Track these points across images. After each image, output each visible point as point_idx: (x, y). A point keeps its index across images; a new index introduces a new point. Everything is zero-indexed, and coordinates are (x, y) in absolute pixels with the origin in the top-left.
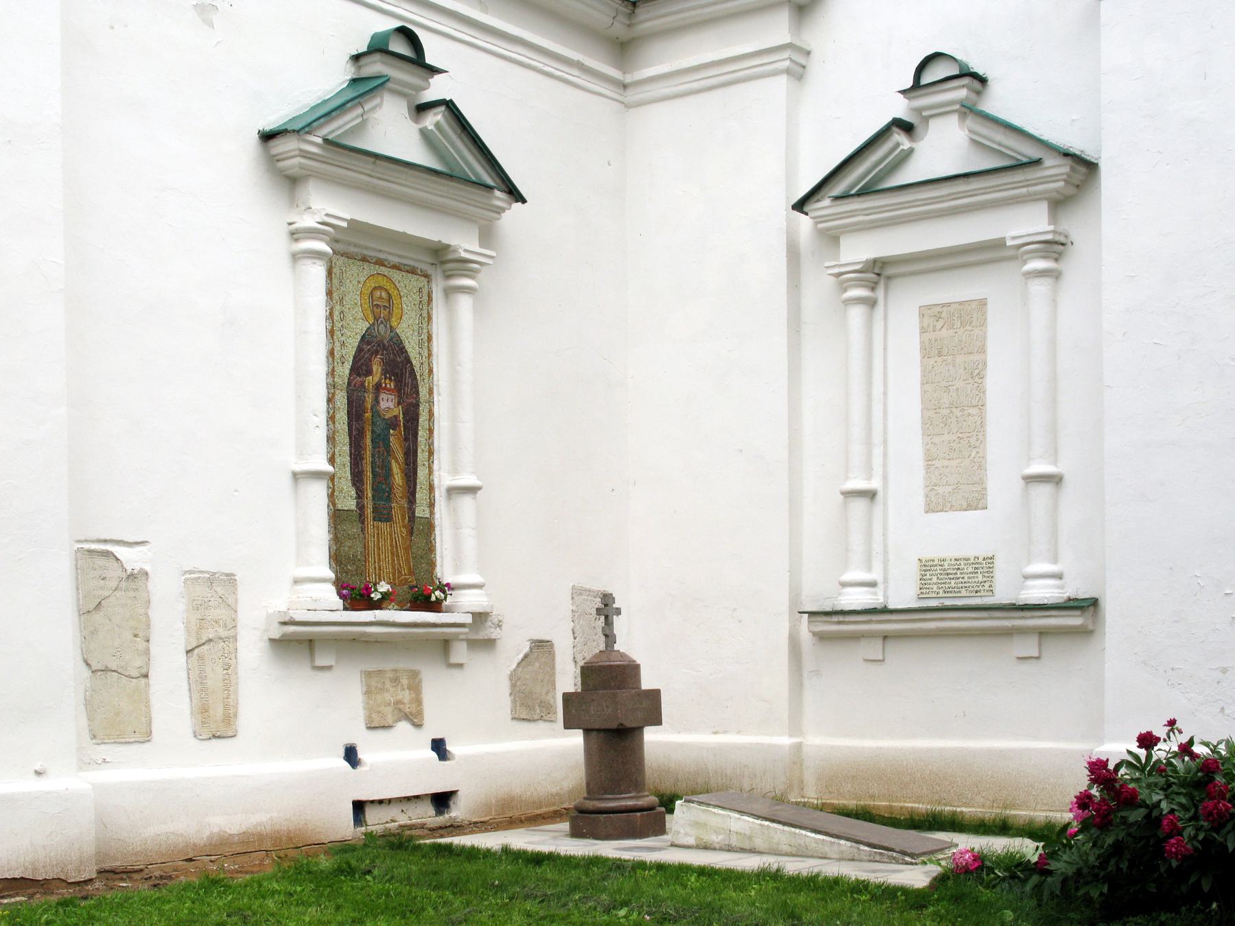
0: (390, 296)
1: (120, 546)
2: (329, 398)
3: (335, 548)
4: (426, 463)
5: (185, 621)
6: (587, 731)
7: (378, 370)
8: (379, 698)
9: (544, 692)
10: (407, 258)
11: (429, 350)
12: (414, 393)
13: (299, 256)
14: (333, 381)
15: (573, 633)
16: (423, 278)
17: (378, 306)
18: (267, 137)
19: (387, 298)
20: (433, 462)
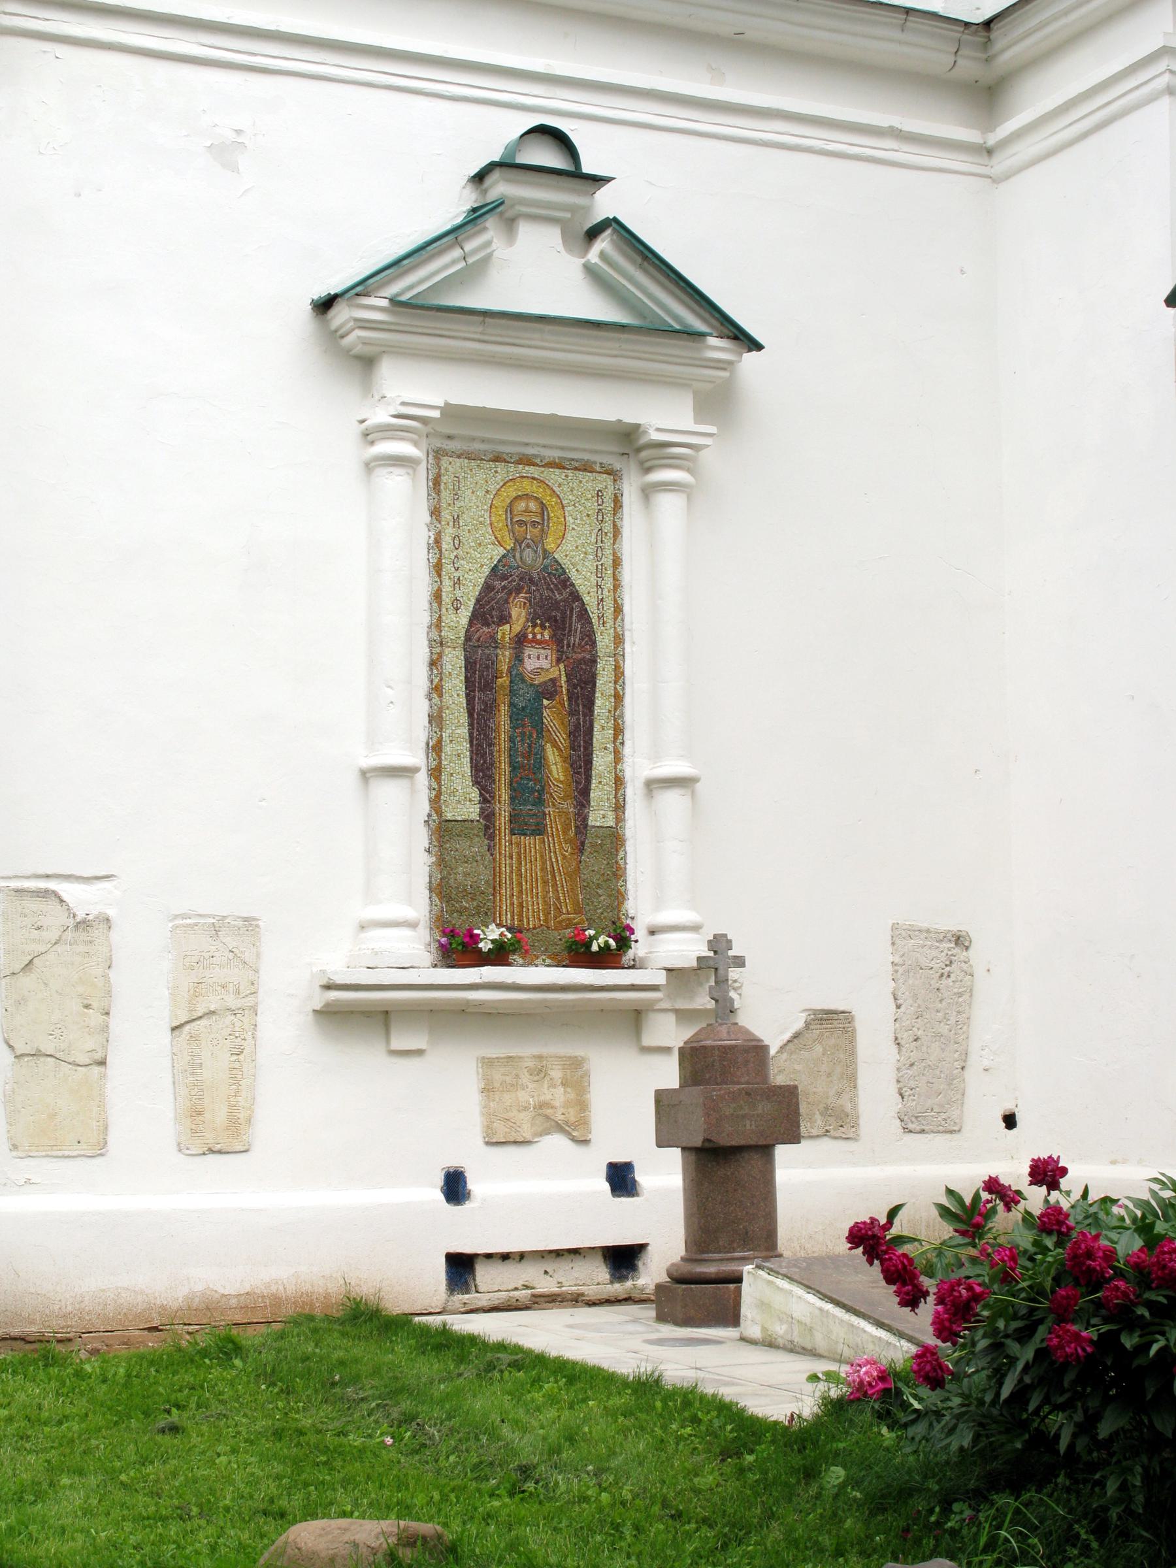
0: (543, 507)
1: (73, 883)
2: (432, 660)
3: (439, 876)
4: (610, 746)
5: (170, 986)
6: (684, 1149)
7: (520, 615)
8: (508, 1098)
9: (832, 1093)
10: (575, 449)
11: (615, 578)
12: (586, 644)
13: (373, 464)
14: (440, 636)
15: (896, 999)
16: (605, 476)
17: (520, 523)
18: (325, 305)
19: (539, 510)
20: (623, 743)
